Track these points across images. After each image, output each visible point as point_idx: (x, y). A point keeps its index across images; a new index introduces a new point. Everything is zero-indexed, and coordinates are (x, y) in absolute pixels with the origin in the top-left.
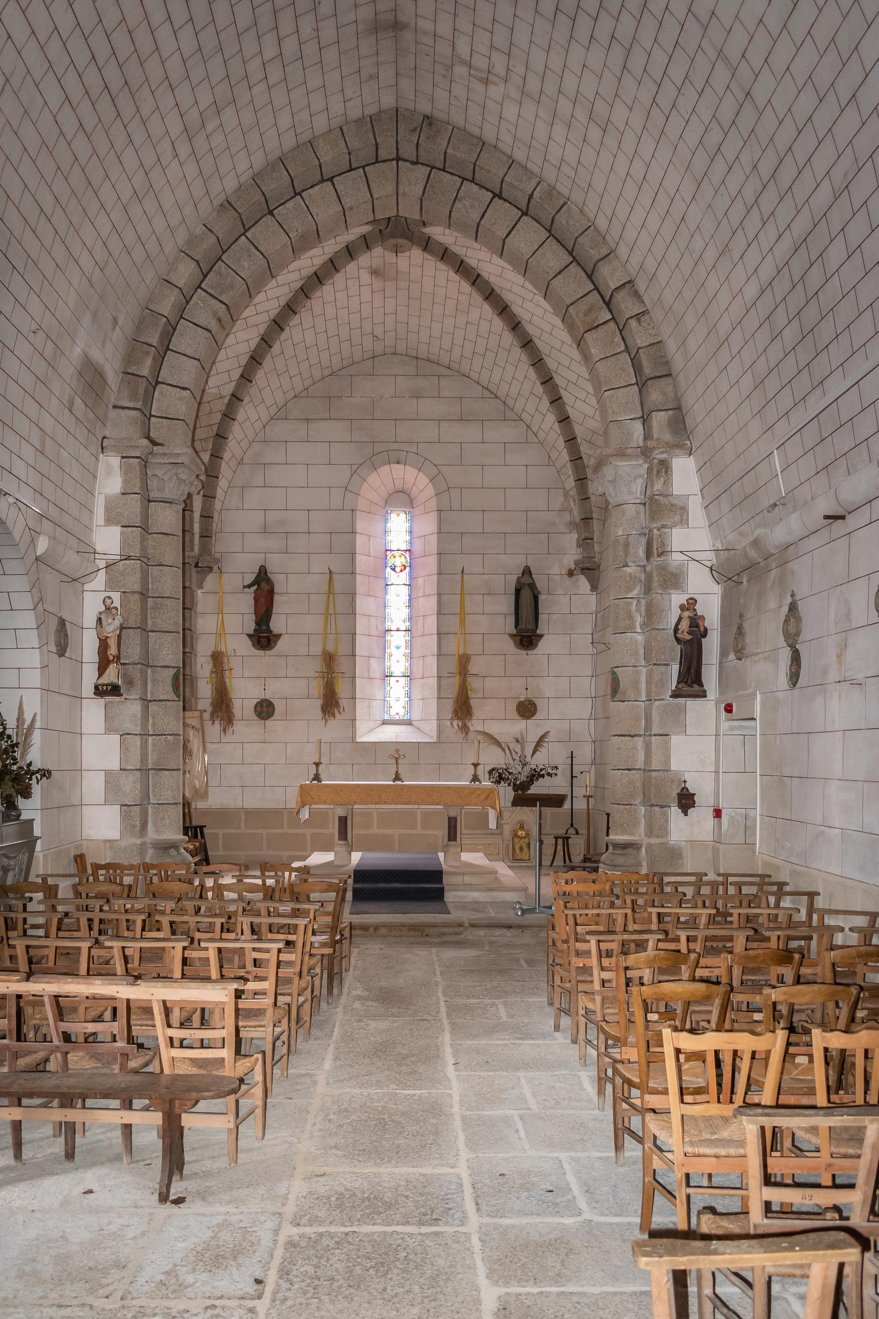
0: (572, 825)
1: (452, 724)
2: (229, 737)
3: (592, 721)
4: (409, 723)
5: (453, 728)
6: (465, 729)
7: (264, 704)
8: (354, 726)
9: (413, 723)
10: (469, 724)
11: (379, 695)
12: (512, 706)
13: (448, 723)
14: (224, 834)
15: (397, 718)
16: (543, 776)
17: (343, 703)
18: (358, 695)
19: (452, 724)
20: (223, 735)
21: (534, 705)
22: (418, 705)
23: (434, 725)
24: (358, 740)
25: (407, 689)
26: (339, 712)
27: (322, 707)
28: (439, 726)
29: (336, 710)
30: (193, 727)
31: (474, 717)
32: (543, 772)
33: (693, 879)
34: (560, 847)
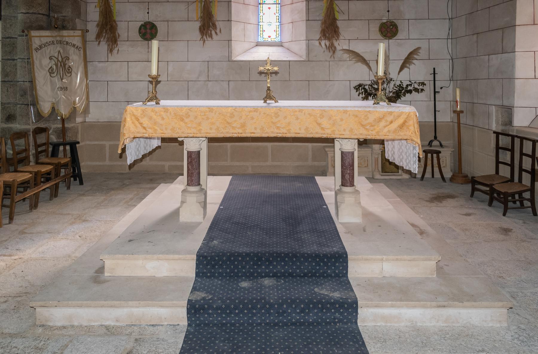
0: (435, 138)
1: (320, 43)
2: (115, 56)
3: (450, 41)
4: (280, 45)
5: (320, 47)
6: (332, 48)
7: (148, 27)
8: (229, 46)
9: (283, 44)
10: (336, 44)
11: (253, 20)
12: (375, 27)
13: (317, 43)
14: (110, 145)
15: (269, 40)
16: (410, 92)
17: (219, 25)
18: (233, 18)
19: (320, 43)
20: (110, 55)
21: (395, 26)
22: (288, 28)
23: (304, 44)
24: (234, 59)
25: (278, 15)
26: (216, 33)
27: (200, 29)
28: (308, 46)
29: (213, 32)
30: (74, 46)
31: (341, 37)
32: (409, 88)
33: (429, 155)
34: (429, 162)
